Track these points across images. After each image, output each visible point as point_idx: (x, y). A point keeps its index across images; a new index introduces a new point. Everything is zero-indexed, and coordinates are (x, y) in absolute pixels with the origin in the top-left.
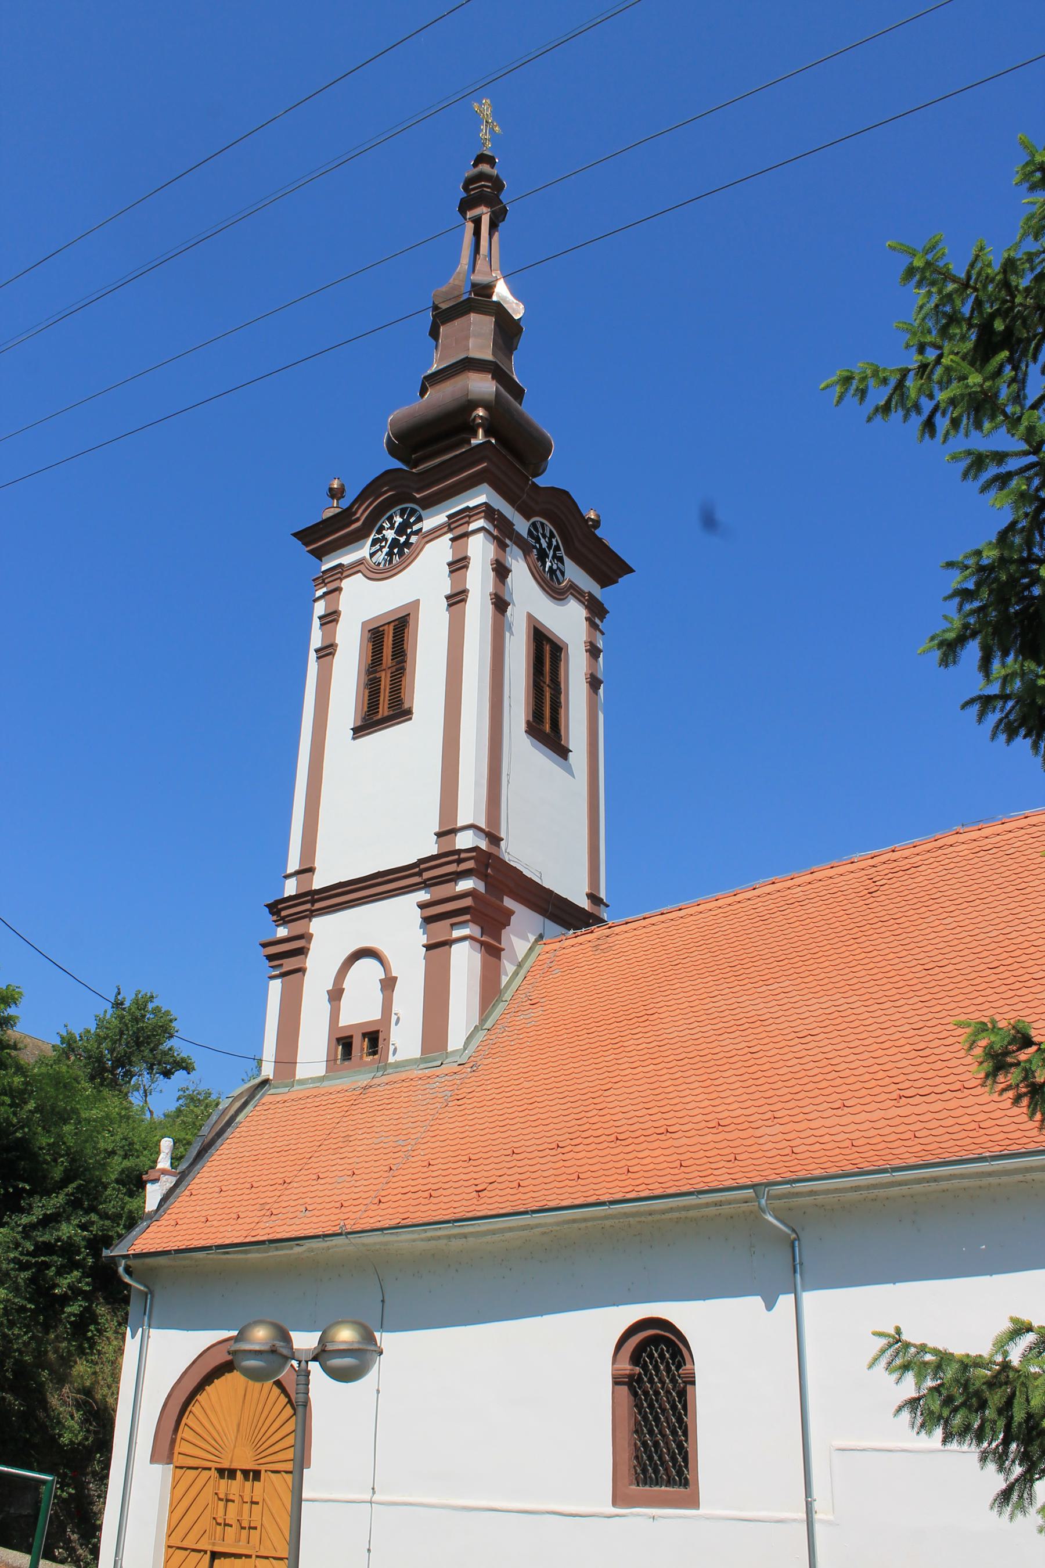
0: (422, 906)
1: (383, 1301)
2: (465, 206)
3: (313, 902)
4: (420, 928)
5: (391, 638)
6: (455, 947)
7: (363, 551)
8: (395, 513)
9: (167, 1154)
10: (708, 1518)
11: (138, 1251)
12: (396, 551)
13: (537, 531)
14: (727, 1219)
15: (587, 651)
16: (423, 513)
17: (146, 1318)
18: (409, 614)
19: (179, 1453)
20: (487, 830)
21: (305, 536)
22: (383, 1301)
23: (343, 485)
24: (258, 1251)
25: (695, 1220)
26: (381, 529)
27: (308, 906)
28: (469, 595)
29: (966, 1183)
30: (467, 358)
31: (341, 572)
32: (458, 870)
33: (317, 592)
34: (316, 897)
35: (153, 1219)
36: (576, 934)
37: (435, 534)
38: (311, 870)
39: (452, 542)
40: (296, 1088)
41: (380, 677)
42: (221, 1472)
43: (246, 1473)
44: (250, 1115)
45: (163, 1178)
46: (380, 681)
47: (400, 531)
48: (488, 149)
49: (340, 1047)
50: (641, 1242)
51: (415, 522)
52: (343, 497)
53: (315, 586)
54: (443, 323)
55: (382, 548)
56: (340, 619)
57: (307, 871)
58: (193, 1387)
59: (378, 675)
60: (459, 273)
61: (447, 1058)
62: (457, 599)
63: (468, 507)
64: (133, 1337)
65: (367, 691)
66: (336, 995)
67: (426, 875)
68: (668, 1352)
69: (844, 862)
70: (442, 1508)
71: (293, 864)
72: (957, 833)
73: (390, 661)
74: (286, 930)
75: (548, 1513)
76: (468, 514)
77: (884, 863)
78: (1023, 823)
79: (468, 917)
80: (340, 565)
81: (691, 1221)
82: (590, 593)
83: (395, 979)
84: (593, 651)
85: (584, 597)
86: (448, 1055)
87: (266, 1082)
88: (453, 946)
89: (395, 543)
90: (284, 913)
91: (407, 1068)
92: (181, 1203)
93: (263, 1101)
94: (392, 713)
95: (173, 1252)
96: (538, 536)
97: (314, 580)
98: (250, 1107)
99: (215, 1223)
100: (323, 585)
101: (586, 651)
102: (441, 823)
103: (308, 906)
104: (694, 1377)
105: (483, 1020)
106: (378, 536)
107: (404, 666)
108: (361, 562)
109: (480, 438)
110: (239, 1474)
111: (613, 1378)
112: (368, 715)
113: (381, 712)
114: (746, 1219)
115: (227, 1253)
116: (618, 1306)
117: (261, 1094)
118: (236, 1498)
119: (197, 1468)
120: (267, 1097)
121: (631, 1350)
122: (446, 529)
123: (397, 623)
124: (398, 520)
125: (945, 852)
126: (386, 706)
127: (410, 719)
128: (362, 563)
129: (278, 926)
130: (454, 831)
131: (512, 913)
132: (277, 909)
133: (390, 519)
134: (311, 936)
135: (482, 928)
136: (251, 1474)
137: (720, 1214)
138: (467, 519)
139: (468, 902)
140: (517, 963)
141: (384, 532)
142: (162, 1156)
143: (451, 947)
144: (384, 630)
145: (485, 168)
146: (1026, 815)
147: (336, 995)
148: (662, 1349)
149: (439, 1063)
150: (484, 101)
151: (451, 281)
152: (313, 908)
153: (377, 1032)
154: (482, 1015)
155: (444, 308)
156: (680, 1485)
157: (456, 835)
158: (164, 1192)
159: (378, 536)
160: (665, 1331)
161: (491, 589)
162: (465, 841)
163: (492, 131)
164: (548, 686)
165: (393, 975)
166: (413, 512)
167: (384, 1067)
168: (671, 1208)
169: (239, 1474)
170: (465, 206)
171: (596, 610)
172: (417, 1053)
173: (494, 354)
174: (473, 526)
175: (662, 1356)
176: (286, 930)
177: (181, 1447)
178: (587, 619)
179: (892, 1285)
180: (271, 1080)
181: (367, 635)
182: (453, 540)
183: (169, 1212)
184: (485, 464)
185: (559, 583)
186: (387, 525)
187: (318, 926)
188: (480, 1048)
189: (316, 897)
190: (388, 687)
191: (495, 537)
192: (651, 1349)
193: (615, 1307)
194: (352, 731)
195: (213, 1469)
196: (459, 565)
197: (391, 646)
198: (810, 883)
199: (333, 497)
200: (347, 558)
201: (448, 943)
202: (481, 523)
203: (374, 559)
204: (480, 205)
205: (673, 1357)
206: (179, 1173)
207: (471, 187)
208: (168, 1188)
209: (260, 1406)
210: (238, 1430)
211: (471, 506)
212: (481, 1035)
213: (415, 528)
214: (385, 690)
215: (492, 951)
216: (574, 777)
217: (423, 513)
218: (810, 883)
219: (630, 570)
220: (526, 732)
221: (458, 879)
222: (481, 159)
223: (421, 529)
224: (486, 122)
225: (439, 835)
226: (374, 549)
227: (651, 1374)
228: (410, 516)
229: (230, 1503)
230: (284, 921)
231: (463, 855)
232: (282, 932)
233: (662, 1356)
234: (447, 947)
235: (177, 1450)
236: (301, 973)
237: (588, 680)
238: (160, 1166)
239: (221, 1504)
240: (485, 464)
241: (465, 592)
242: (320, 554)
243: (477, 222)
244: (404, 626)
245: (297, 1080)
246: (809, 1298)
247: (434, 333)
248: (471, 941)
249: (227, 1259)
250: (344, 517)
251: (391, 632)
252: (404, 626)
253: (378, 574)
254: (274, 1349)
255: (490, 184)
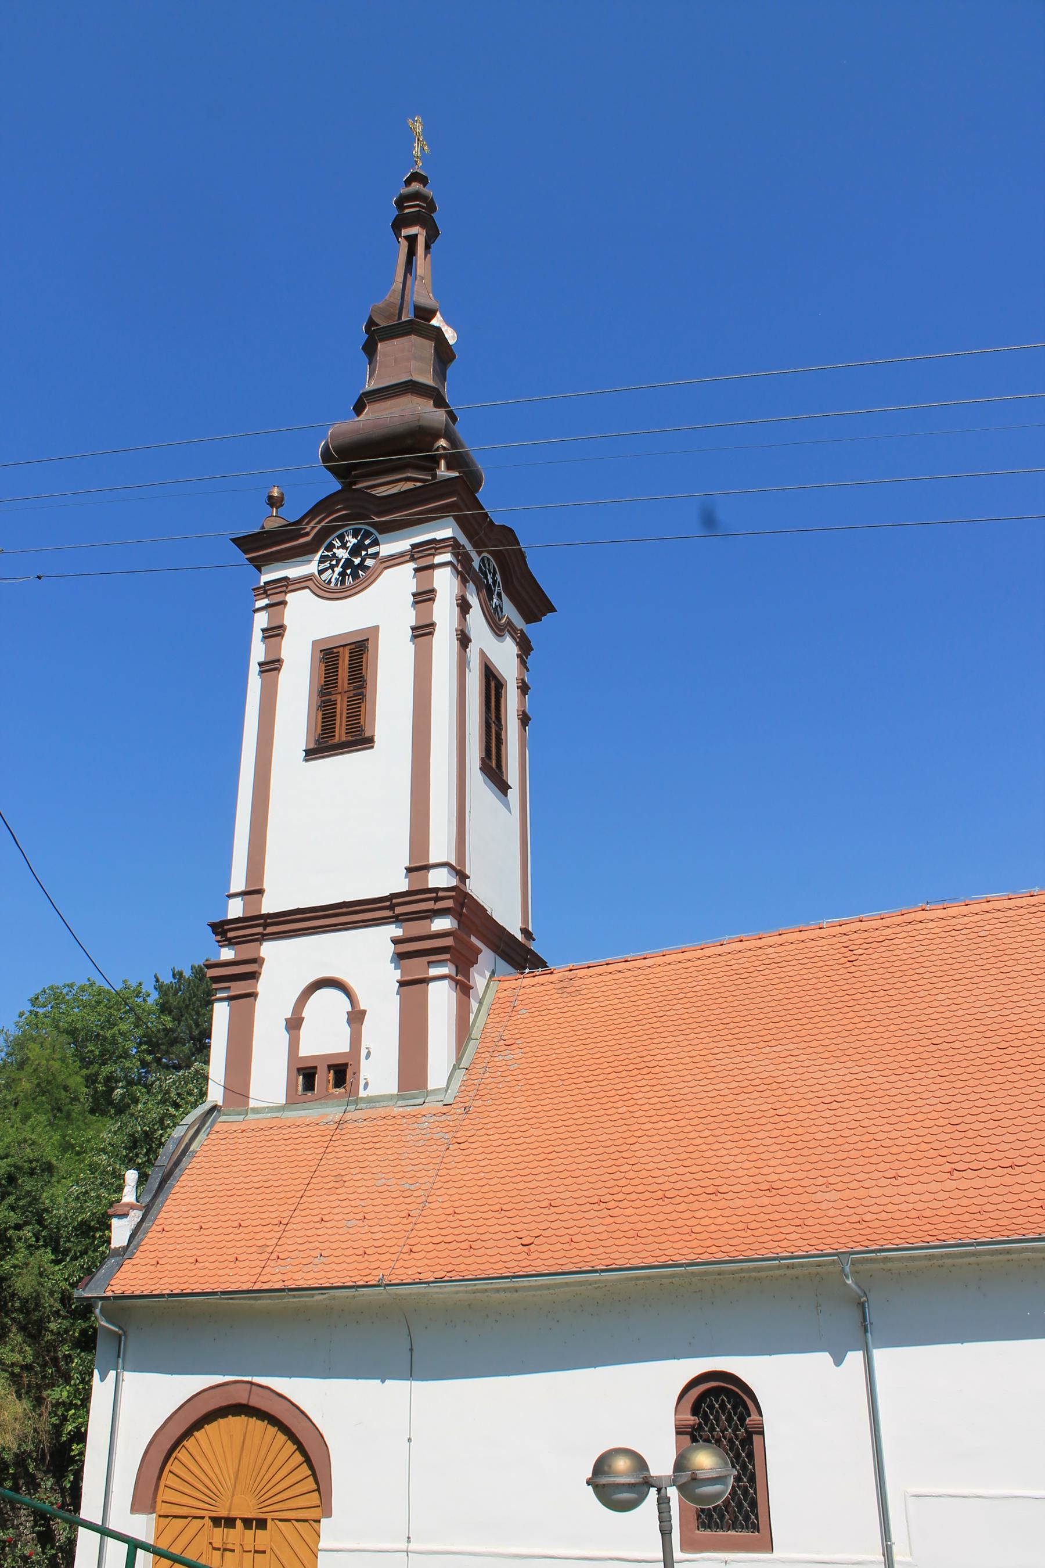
0: (396, 941)
1: (411, 1350)
2: (398, 225)
3: (265, 926)
4: (391, 963)
5: (347, 662)
6: (432, 986)
7: (311, 567)
8: (346, 532)
9: (133, 1187)
10: (783, 1561)
11: (118, 1292)
12: (349, 571)
13: (485, 567)
14: (792, 1279)
15: (518, 687)
16: (380, 537)
17: (120, 1361)
18: (368, 639)
19: (163, 1502)
20: (458, 868)
21: (244, 543)
22: (411, 1350)
23: (282, 494)
24: (270, 1298)
25: (759, 1279)
26: (330, 547)
27: (260, 930)
28: (436, 629)
29: (1030, 1255)
30: (411, 381)
31: (285, 585)
32: (435, 908)
33: (257, 602)
34: (269, 921)
35: (125, 1257)
36: (534, 974)
37: (394, 560)
38: (260, 892)
39: (415, 572)
40: (250, 1116)
41: (336, 700)
42: (216, 1521)
43: (247, 1523)
44: (205, 1143)
45: (132, 1213)
46: (336, 704)
47: (355, 551)
48: (419, 168)
49: (301, 1077)
50: (702, 1299)
51: (371, 545)
52: (282, 506)
53: (255, 596)
54: (382, 340)
55: (332, 567)
56: (286, 634)
57: (254, 892)
58: (180, 1434)
59: (333, 698)
60: (394, 291)
61: (427, 1096)
62: (423, 631)
63: (435, 539)
64: (102, 1379)
65: (320, 713)
66: (294, 1024)
67: (399, 910)
68: (729, 1402)
69: (812, 927)
70: (491, 1556)
71: (238, 883)
72: (923, 910)
73: (346, 685)
74: (233, 952)
75: (611, 1559)
76: (434, 546)
77: (855, 932)
78: (986, 906)
79: (448, 956)
80: (286, 579)
81: (755, 1280)
82: (522, 630)
83: (364, 1012)
84: (524, 688)
85: (517, 634)
86: (428, 1093)
87: (214, 1108)
88: (430, 984)
89: (348, 563)
90: (230, 935)
91: (382, 1104)
92: (151, 1239)
93: (217, 1128)
94: (350, 738)
95: (166, 1296)
96: (486, 571)
97: (253, 590)
98: (202, 1136)
99: (207, 1264)
100: (264, 596)
101: (518, 687)
102: (411, 858)
103: (260, 930)
104: (763, 1428)
105: (459, 1059)
106: (326, 553)
107: (363, 692)
108: (309, 578)
109: (443, 470)
110: (239, 1523)
111: (676, 1428)
112: (322, 738)
113: (337, 736)
114: (811, 1280)
115: (231, 1299)
116: (679, 1359)
117: (210, 1120)
118: (238, 1549)
119: (186, 1517)
120: (222, 1123)
121: (693, 1401)
122: (408, 558)
123: (353, 646)
124: (352, 541)
125: (916, 927)
126: (344, 731)
127: (372, 747)
128: (311, 579)
129: (221, 946)
130: (427, 867)
131: (480, 951)
132: (222, 930)
133: (341, 538)
134: (263, 960)
135: (457, 967)
136: (254, 1522)
137: (785, 1275)
138: (433, 551)
139: (449, 941)
140: (478, 1000)
141: (335, 550)
142: (126, 1190)
143: (428, 985)
144: (338, 652)
145: (416, 186)
146: (988, 900)
147: (294, 1024)
148: (723, 1400)
149: (421, 1101)
150: (416, 119)
151: (387, 297)
152: (265, 932)
153: (346, 1065)
154: (459, 1053)
155: (382, 326)
156: (743, 1528)
157: (428, 872)
158: (133, 1227)
159: (326, 553)
160: (727, 1384)
161: (456, 625)
162: (440, 879)
163: (422, 149)
164: (494, 722)
165: (362, 1008)
166: (367, 534)
167: (351, 1097)
168: (742, 1269)
169: (239, 1523)
170: (398, 225)
171: (525, 647)
172: (394, 1090)
173: (434, 380)
174: (438, 559)
175: (723, 1406)
176: (233, 952)
177: (164, 1494)
178: (518, 656)
179: (960, 1344)
180: (221, 1107)
181: (319, 655)
182: (416, 570)
183: (141, 1248)
184: (455, 499)
185: (500, 620)
186: (337, 543)
187: (268, 950)
188: (463, 1088)
189: (269, 921)
190: (345, 712)
191: (458, 573)
192: (711, 1400)
193: (676, 1360)
194: (304, 753)
195: (207, 1518)
196: (424, 597)
197: (347, 670)
198: (781, 945)
199: (272, 505)
200: (294, 572)
201: (426, 981)
202: (447, 557)
203: (324, 576)
204: (415, 225)
205: (735, 1408)
206: (144, 1207)
207: (405, 204)
208: (136, 1223)
209: (263, 1453)
210: (236, 1478)
211: (438, 538)
212: (460, 1075)
213: (371, 551)
214: (341, 714)
215: (464, 989)
216: (511, 813)
217: (380, 537)
218: (781, 945)
219: (554, 610)
220: (480, 768)
221: (435, 916)
222: (415, 177)
223: (378, 553)
224: (418, 140)
225: (409, 870)
226: (322, 566)
227: (712, 1424)
228: (365, 537)
229: (227, 1553)
230: (230, 943)
231: (441, 894)
232: (227, 954)
233: (723, 1406)
234: (426, 984)
235: (159, 1498)
236: (253, 998)
237: (521, 717)
238: (125, 1200)
239: (218, 1553)
240: (455, 499)
241: (432, 625)
242: (259, 564)
243: (412, 240)
244: (362, 650)
245: (251, 1108)
246: (879, 1355)
247: (370, 349)
248: (450, 981)
249: (233, 1303)
250: (290, 532)
251: (347, 656)
252: (362, 650)
253: (327, 592)
254: (694, 1477)
255: (425, 205)
